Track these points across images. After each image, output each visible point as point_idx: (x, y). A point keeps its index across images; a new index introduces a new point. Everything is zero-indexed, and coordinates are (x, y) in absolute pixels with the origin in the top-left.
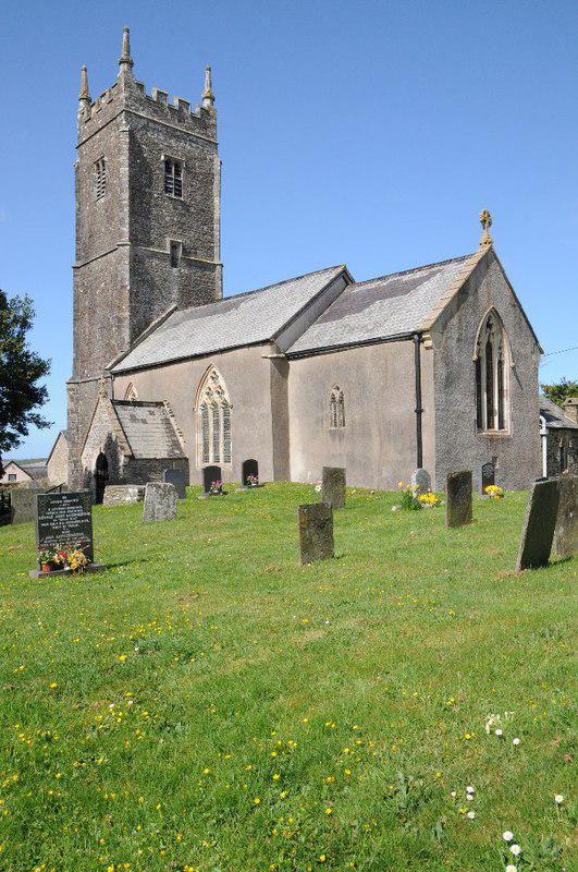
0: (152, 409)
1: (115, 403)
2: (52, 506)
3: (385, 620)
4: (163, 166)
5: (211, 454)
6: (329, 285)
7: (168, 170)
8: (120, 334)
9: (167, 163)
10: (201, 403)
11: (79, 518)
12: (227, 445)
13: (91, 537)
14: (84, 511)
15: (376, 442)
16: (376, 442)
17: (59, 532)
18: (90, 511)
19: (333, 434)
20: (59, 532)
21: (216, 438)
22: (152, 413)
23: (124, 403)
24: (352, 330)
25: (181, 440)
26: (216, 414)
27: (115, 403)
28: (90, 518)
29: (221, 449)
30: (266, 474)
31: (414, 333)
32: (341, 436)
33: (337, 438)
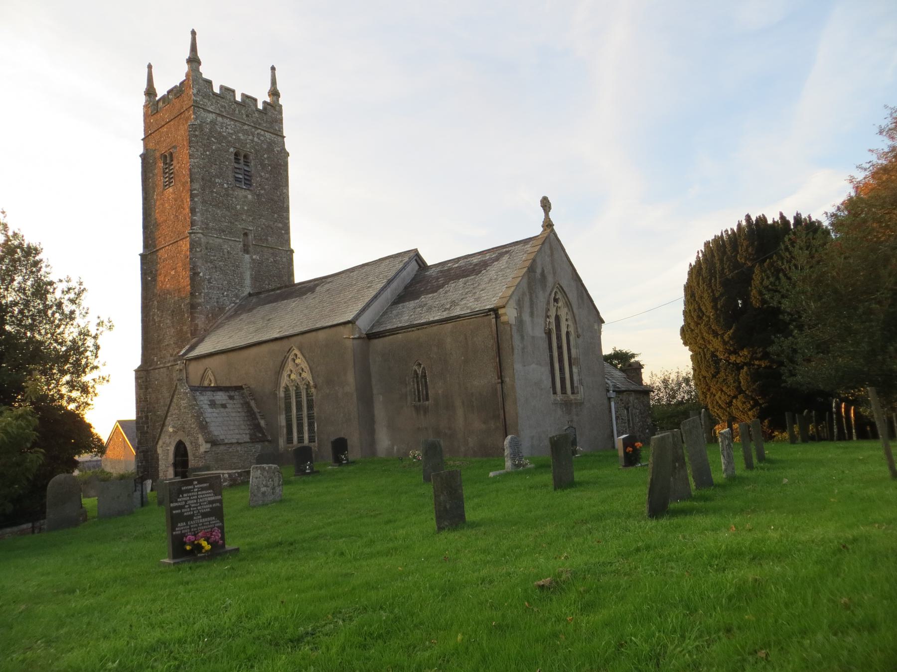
0: (232, 394)
1: (194, 389)
2: (182, 492)
3: (250, 618)
4: (232, 157)
5: (306, 436)
6: (403, 268)
7: (237, 160)
8: (193, 319)
9: (237, 155)
10: (283, 385)
11: (211, 502)
12: (311, 425)
13: (222, 521)
14: (216, 495)
15: (460, 412)
16: (460, 412)
17: (190, 518)
18: (220, 494)
19: (417, 409)
20: (190, 518)
21: (300, 419)
22: (231, 398)
23: (203, 389)
24: (430, 309)
25: (262, 423)
26: (298, 395)
27: (194, 389)
28: (220, 501)
29: (306, 428)
30: (354, 452)
31: (490, 310)
32: (426, 410)
33: (422, 412)
